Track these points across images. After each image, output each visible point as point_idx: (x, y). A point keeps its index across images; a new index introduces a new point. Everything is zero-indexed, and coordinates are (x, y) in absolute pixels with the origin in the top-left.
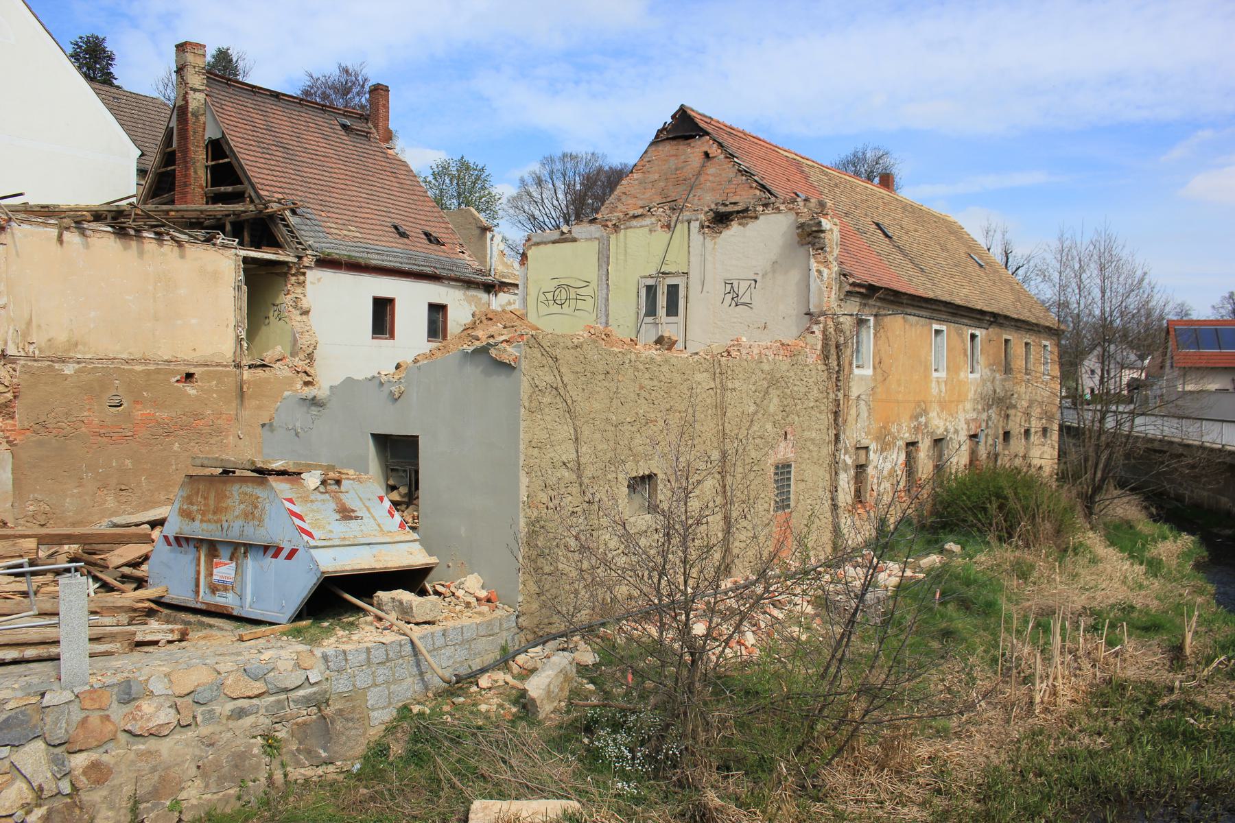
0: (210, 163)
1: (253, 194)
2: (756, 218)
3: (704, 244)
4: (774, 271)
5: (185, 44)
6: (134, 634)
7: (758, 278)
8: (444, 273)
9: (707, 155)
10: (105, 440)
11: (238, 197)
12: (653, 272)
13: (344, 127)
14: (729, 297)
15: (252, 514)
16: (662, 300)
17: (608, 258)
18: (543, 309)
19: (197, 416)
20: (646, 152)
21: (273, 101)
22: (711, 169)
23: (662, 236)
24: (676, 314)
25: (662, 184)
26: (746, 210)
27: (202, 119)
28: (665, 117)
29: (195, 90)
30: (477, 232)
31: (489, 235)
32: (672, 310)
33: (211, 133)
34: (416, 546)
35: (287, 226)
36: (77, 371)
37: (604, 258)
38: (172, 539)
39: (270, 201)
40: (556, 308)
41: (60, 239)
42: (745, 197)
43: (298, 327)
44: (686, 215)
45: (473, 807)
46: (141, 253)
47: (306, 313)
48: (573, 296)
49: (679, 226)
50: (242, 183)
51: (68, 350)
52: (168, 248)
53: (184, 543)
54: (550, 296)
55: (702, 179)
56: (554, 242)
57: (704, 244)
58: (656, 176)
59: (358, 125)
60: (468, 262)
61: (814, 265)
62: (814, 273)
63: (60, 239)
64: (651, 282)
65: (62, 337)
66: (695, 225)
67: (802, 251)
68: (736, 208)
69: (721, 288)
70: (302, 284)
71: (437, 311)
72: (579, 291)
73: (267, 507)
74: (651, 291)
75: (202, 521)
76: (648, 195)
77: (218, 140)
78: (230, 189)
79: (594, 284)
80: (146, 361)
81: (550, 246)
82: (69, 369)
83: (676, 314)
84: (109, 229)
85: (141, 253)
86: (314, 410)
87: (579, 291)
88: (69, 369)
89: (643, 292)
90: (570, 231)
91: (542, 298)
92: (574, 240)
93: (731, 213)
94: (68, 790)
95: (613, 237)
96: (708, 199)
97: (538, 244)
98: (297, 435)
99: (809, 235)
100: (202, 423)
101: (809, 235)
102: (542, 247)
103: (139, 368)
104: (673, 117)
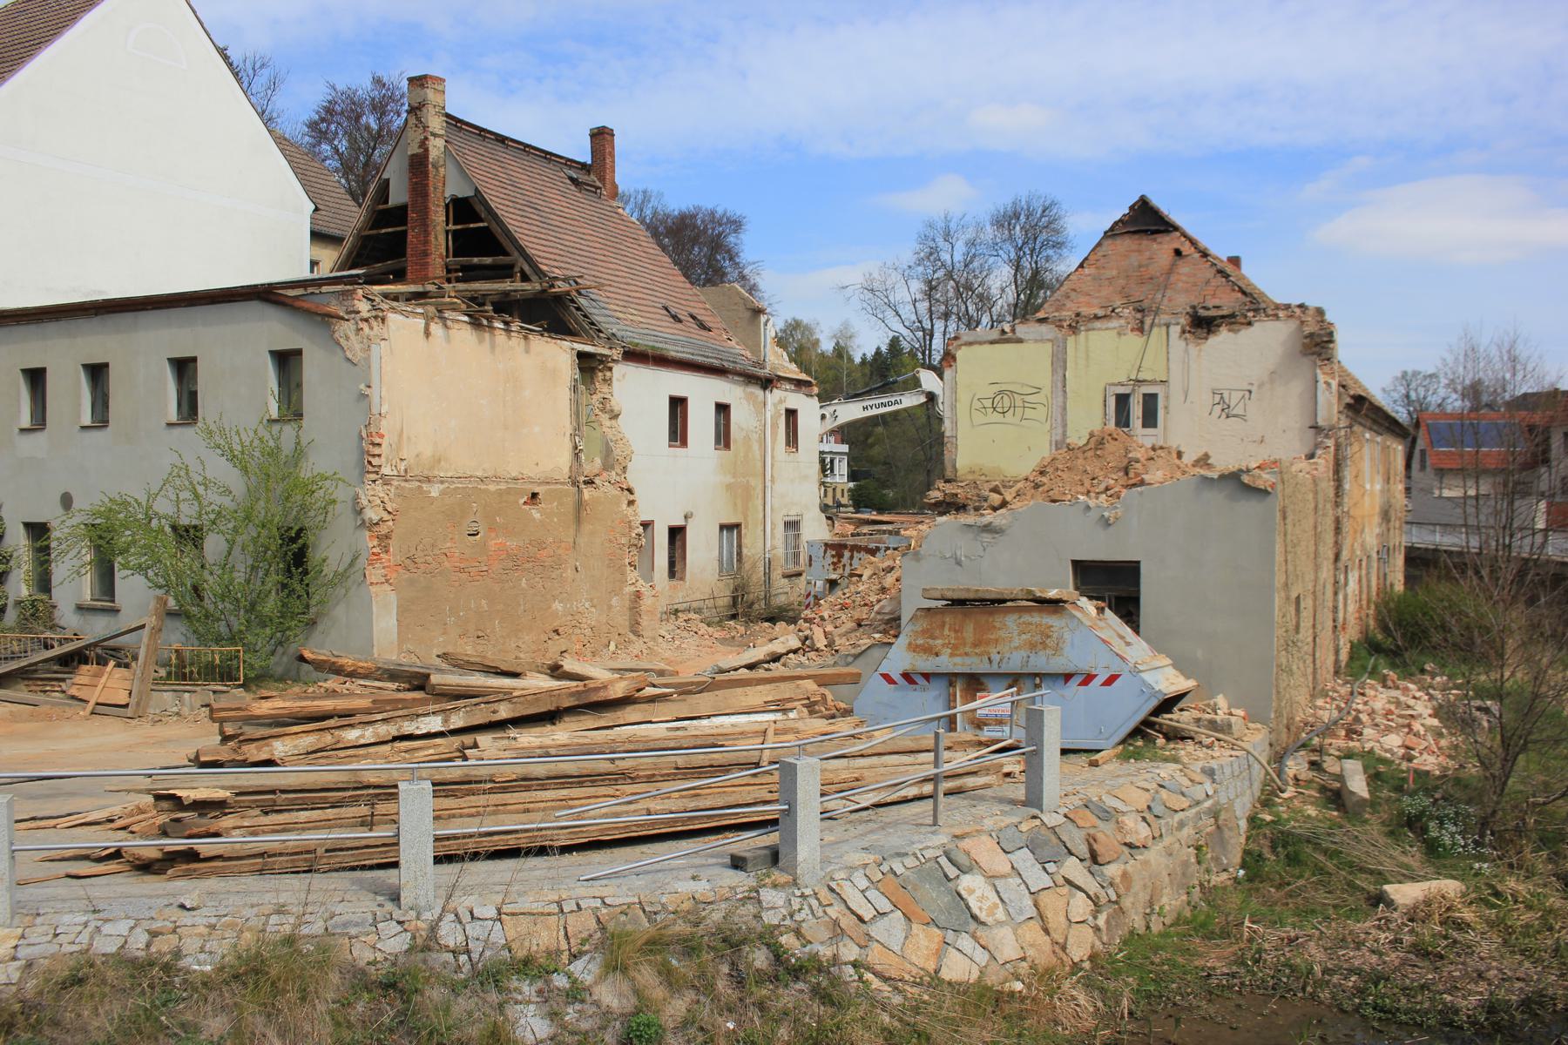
0: (451, 227)
1: (526, 268)
2: (1250, 324)
3: (1186, 351)
4: (1272, 381)
5: (424, 77)
6: (1002, 766)
7: (1254, 389)
8: (731, 366)
9: (1178, 253)
10: (464, 576)
11: (505, 272)
12: (1123, 379)
13: (571, 179)
14: (1218, 408)
15: (1042, 642)
16: (1136, 410)
17: (1065, 362)
18: (978, 418)
19: (541, 545)
20: (1099, 244)
21: (499, 147)
22: (1184, 268)
23: (1135, 340)
24: (1155, 425)
25: (1122, 282)
26: (1233, 316)
27: (442, 170)
28: (1119, 210)
29: (435, 135)
30: (748, 314)
31: (763, 318)
32: (1150, 419)
33: (455, 188)
34: (1171, 671)
35: (578, 309)
36: (443, 493)
37: (1059, 362)
38: (896, 676)
39: (556, 278)
40: (997, 417)
41: (427, 333)
42: (1227, 301)
43: (610, 434)
44: (1164, 318)
45: (947, 978)
46: (493, 346)
47: (615, 417)
48: (1019, 403)
49: (1155, 330)
50: (506, 254)
51: (432, 468)
52: (516, 342)
53: (921, 681)
54: (988, 403)
55: (1173, 278)
56: (992, 343)
57: (1186, 351)
58: (1114, 273)
59: (582, 177)
60: (735, 349)
61: (1321, 378)
62: (1321, 386)
63: (427, 333)
64: (1121, 390)
65: (428, 452)
66: (1175, 330)
67: (1306, 362)
68: (1220, 313)
69: (1208, 399)
70: (608, 381)
71: (723, 409)
72: (1028, 398)
73: (1067, 636)
74: (1123, 401)
75: (952, 655)
76: (1104, 293)
77: (465, 200)
78: (488, 260)
79: (1047, 390)
80: (497, 478)
81: (987, 347)
82: (435, 491)
83: (1155, 425)
84: (466, 319)
85: (493, 346)
86: (987, 537)
87: (1028, 398)
88: (435, 491)
89: (1112, 402)
90: (1013, 331)
91: (977, 405)
92: (1020, 341)
93: (1214, 318)
94: (1114, 898)
95: (1071, 340)
96: (1181, 301)
97: (970, 344)
98: (959, 563)
99: (1317, 345)
100: (544, 553)
101: (1317, 345)
102: (976, 347)
103: (492, 487)
104: (1131, 208)
